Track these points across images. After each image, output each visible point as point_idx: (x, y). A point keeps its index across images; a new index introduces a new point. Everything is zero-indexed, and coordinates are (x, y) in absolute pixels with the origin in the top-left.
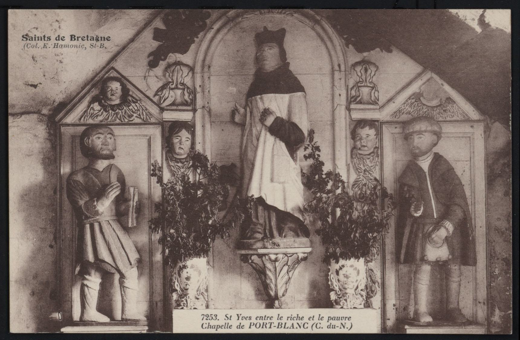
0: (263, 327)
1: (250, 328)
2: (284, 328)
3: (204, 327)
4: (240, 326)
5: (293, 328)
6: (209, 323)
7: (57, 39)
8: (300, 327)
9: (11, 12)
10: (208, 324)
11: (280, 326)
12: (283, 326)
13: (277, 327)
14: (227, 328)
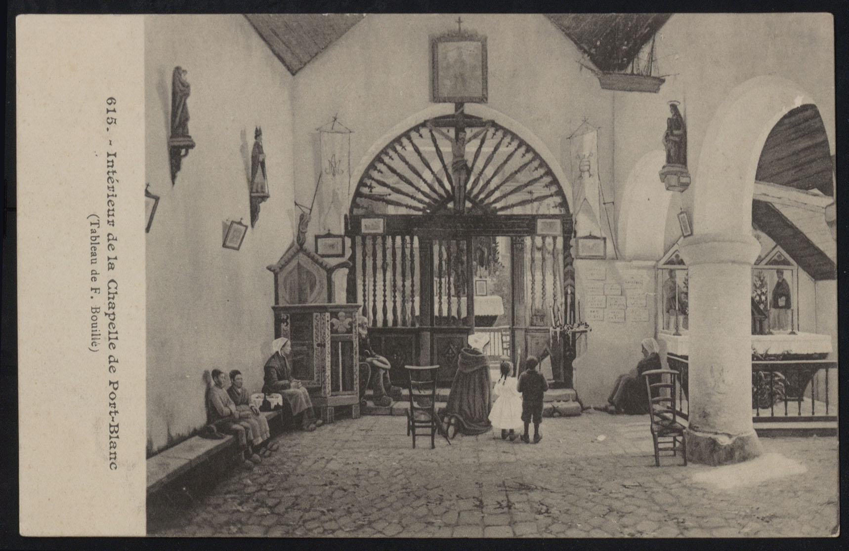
7: (94, 272)
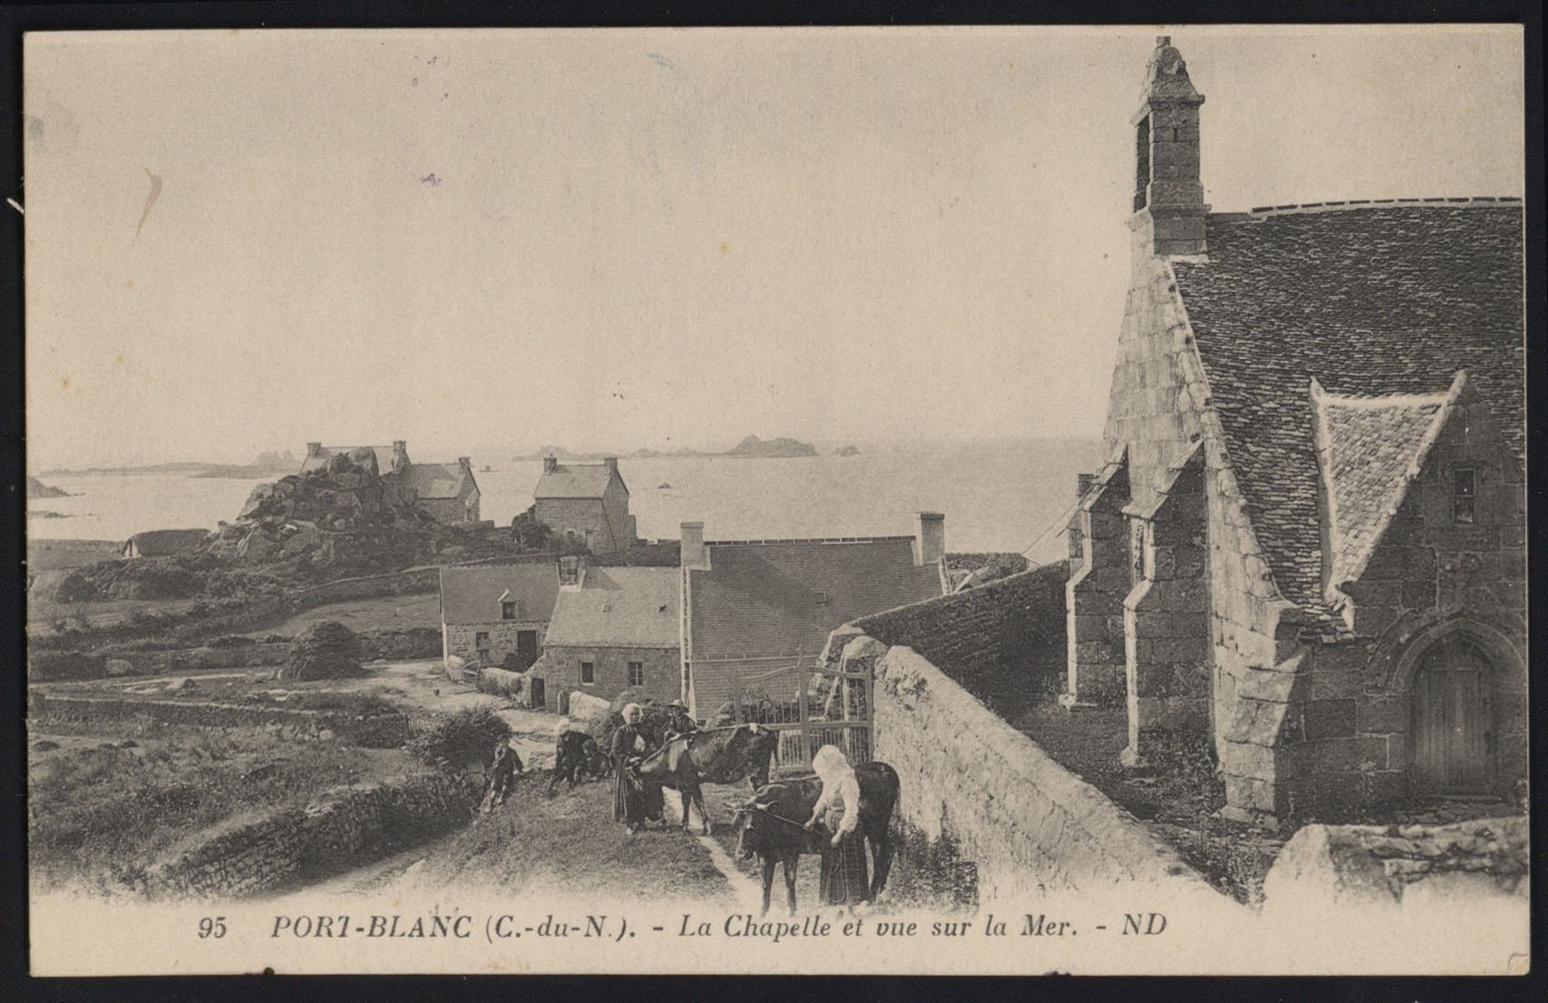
0: (318, 934)
1: (275, 935)
2: (392, 935)
3: (732, 930)
4: (548, 926)
5: (421, 935)
6: (750, 917)
8: (444, 932)
9: (1521, 967)
10: (745, 920)
11: (377, 930)
12: (388, 927)
13: (367, 931)
14: (754, 934)
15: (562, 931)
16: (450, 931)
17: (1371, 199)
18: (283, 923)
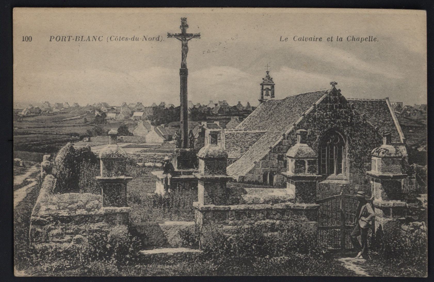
0: (62, 40)
1: (51, 41)
10: (352, 37)
11: (77, 40)
15: (137, 39)
16: (97, 39)
17: (351, 98)
18: (52, 38)
